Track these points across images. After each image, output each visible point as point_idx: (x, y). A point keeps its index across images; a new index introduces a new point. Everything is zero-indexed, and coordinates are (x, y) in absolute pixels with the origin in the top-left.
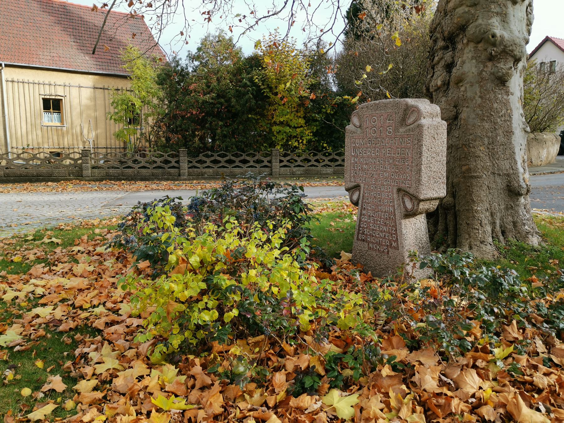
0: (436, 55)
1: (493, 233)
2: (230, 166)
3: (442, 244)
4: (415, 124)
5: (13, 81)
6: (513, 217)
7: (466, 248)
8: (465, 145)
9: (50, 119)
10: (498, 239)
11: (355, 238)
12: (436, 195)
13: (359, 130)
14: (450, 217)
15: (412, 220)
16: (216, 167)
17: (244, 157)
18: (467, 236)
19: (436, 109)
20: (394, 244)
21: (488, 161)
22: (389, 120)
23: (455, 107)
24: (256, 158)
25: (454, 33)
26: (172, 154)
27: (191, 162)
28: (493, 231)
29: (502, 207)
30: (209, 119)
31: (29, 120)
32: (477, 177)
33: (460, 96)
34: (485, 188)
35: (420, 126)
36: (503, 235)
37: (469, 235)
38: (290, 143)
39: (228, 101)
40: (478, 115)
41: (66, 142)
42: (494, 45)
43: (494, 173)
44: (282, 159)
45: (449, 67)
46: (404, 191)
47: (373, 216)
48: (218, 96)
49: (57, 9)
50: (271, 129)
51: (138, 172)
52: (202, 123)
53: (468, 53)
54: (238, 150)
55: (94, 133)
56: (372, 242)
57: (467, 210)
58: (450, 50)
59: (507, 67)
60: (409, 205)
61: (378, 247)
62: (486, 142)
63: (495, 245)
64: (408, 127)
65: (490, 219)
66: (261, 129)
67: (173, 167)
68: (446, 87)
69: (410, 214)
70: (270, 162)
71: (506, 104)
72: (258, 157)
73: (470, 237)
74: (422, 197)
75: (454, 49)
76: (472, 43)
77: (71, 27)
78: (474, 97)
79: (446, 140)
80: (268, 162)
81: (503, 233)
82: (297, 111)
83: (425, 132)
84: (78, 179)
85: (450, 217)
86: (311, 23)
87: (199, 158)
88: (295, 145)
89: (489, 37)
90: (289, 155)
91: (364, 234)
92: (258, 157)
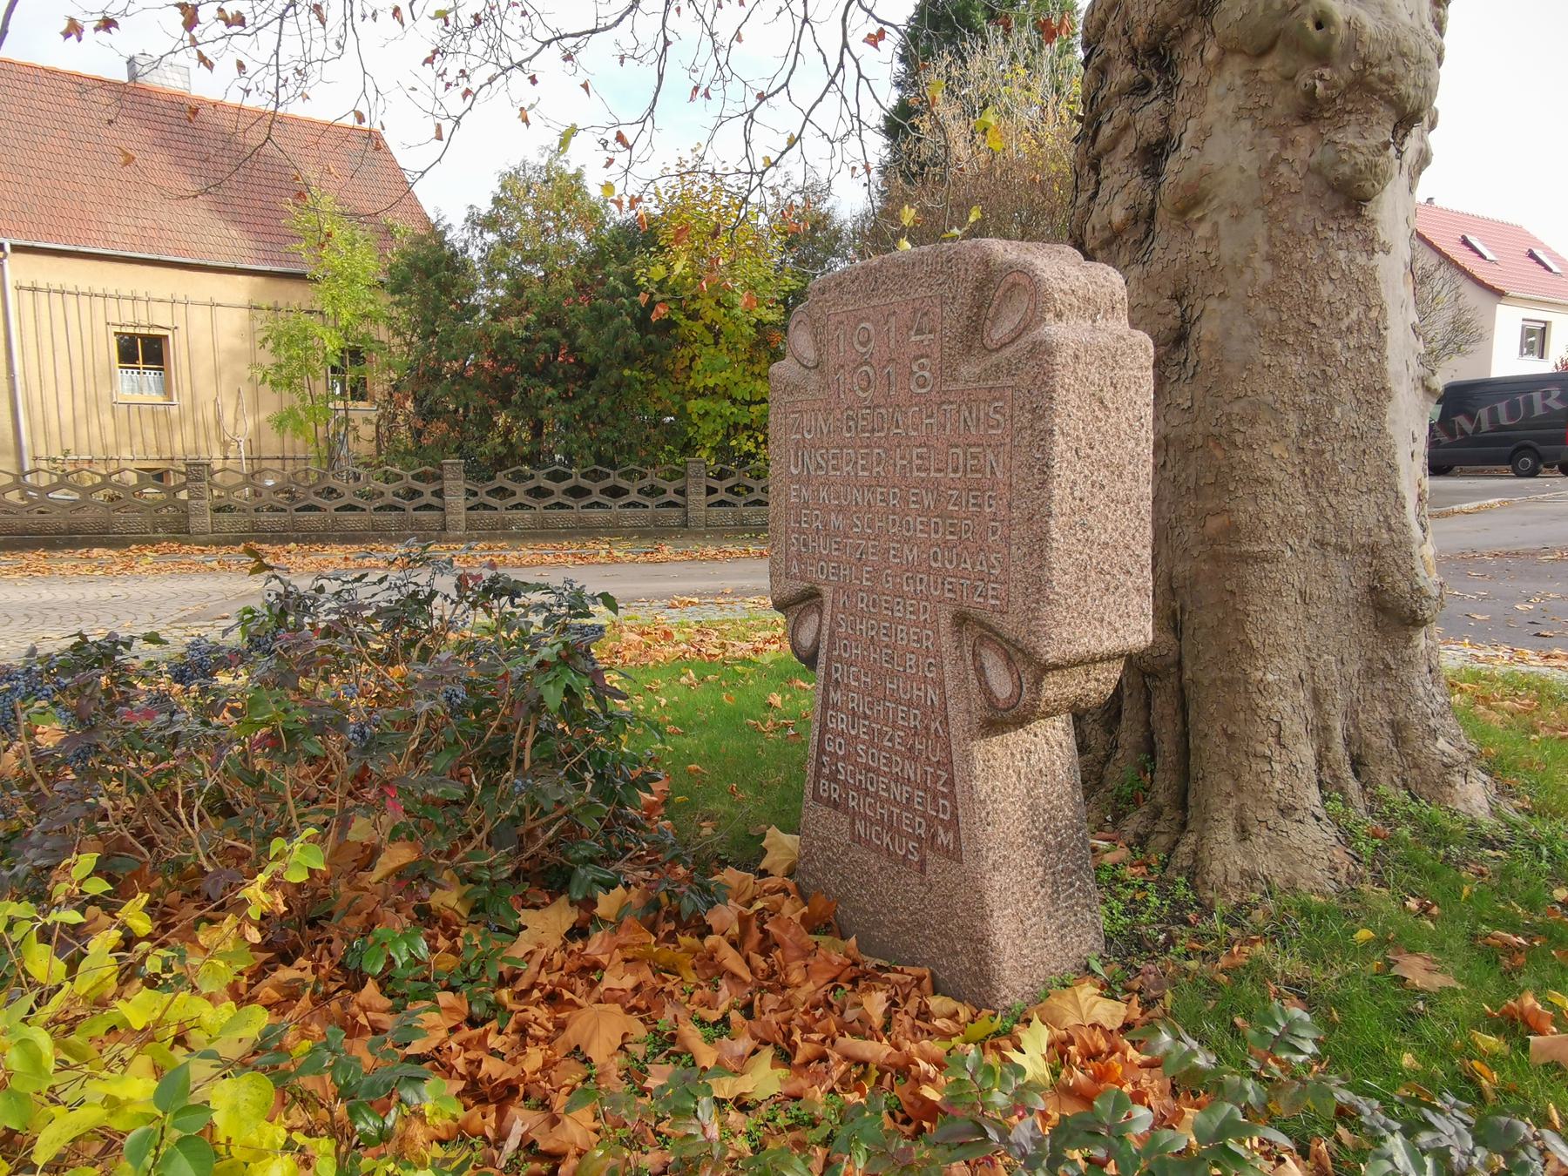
0: (1104, 118)
1: (1320, 768)
2: (577, 504)
3: (1134, 801)
4: (1021, 342)
5: (34, 289)
6: (1391, 703)
7: (1225, 833)
8: (1216, 438)
9: (136, 385)
10: (1341, 790)
11: (808, 791)
12: (1110, 644)
13: (814, 376)
14: (1163, 705)
15: (1017, 738)
16: (539, 504)
17: (615, 479)
18: (1228, 785)
19: (1109, 280)
20: (944, 838)
21: (1300, 499)
22: (919, 332)
23: (1178, 297)
24: (646, 483)
25: (1168, 27)
26: (425, 473)
27: (475, 494)
28: (1320, 760)
29: (1353, 668)
30: (521, 382)
31: (79, 389)
32: (1258, 559)
33: (1195, 256)
34: (1290, 598)
35: (1042, 352)
36: (1357, 774)
37: (1236, 779)
38: (734, 443)
39: (570, 335)
40: (1260, 324)
41: (182, 443)
42: (1322, 56)
43: (1323, 544)
44: (714, 484)
45: (1153, 155)
46: (982, 624)
47: (866, 717)
48: (546, 321)
49: (160, 111)
50: (683, 408)
51: (335, 521)
52: (502, 391)
53: (1222, 98)
54: (599, 462)
55: (250, 423)
56: (865, 817)
57: (1229, 683)
58: (1153, 94)
59: (1372, 142)
60: (1001, 684)
61: (887, 839)
62: (1293, 429)
63: (1335, 819)
64: (994, 358)
65: (1310, 714)
66: (659, 408)
67: (428, 507)
68: (1142, 227)
69: (1001, 719)
70: (681, 492)
71: (1365, 287)
72: (653, 478)
73: (1240, 789)
74: (1051, 656)
75: (1170, 89)
76: (1238, 59)
77: (197, 156)
78: (1248, 260)
79: (1150, 411)
80: (676, 492)
81: (1357, 764)
82: (751, 361)
83: (1064, 377)
84: (175, 540)
85: (1163, 705)
86: (726, 69)
87: (496, 484)
88: (746, 448)
89: (1303, 26)
90: (732, 474)
91: (836, 781)
92: (653, 478)
